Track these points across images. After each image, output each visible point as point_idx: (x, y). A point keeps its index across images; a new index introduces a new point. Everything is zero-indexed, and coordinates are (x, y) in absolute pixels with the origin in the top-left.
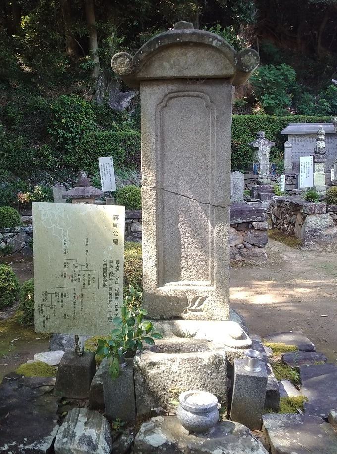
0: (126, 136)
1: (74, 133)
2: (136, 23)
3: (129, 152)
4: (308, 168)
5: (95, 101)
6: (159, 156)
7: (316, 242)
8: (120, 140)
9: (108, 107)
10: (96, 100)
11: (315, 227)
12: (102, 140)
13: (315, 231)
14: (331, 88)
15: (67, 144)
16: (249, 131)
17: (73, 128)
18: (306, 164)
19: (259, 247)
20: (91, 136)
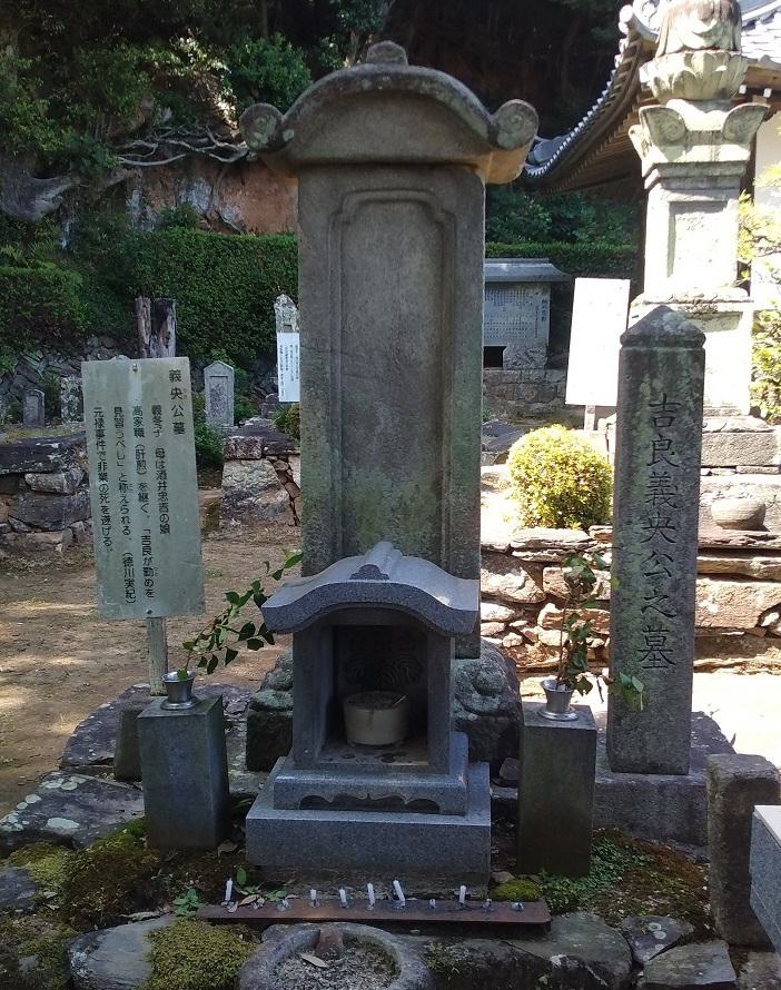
7: (243, 521)
11: (238, 487)
13: (241, 496)
18: (289, 349)
19: (45, 530)
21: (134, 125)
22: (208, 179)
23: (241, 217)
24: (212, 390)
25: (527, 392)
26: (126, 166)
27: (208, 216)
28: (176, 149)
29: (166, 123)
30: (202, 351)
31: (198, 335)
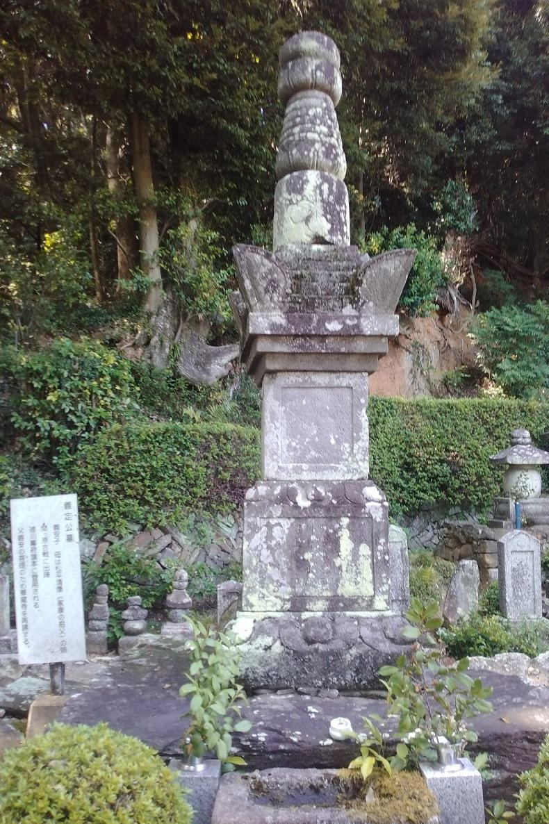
0: (209, 433)
1: (76, 427)
2: (242, 202)
3: (217, 473)
5: (149, 361)
6: (28, 115)
8: (193, 442)
9: (177, 375)
10: (150, 358)
12: (145, 442)
15: (58, 454)
16: (483, 430)
17: (75, 415)
18: (40, 536)
20: (118, 433)
24: (514, 570)
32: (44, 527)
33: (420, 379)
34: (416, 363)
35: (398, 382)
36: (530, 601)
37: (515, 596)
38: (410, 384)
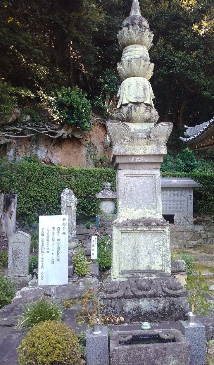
4: (56, 242)
14: (187, 151)
18: (51, 231)
21: (11, 120)
22: (46, 146)
23: (60, 161)
24: (14, 251)
25: (188, 236)
26: (7, 137)
27: (45, 160)
28: (33, 132)
29: (27, 122)
30: (34, 219)
31: (32, 212)
32: (53, 228)
33: (89, 159)
34: (89, 152)
35: (79, 161)
36: (22, 267)
37: (14, 264)
38: (85, 161)
